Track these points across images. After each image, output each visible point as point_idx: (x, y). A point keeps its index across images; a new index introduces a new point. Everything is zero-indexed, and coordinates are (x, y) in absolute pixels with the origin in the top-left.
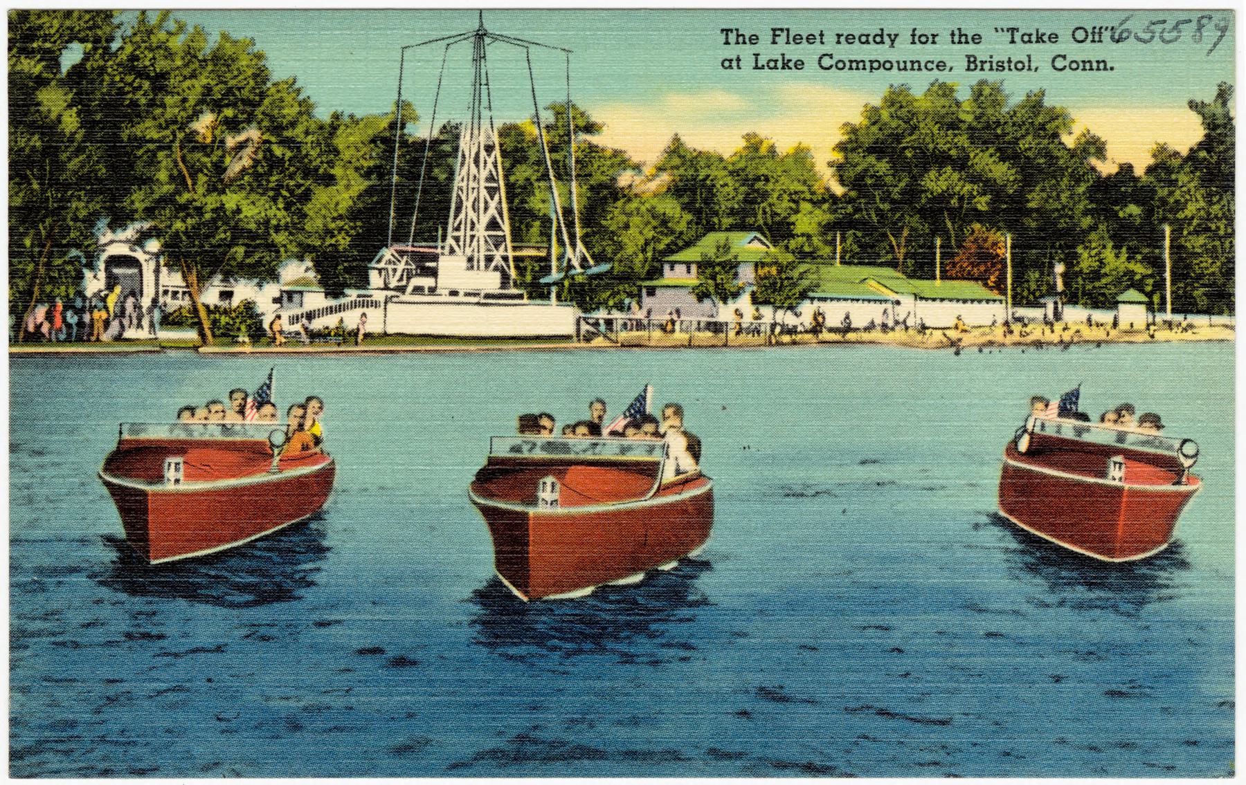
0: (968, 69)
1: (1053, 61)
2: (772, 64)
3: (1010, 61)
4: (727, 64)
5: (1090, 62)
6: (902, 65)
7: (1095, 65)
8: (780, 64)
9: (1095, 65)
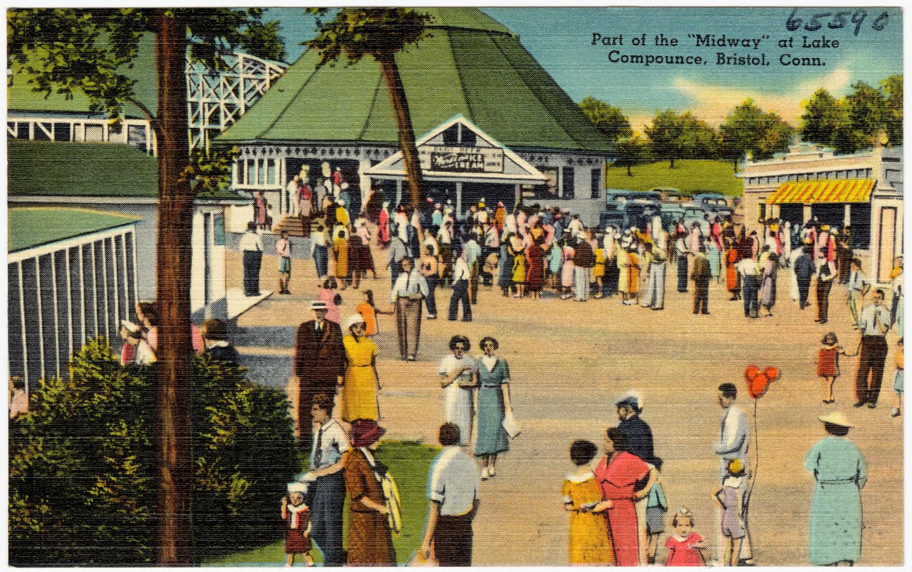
0: (719, 63)
1: (781, 59)
2: (816, 44)
3: (749, 59)
4: (782, 43)
5: (682, 58)
6: (806, 62)
7: (811, 62)
8: (821, 44)
9: (811, 62)
